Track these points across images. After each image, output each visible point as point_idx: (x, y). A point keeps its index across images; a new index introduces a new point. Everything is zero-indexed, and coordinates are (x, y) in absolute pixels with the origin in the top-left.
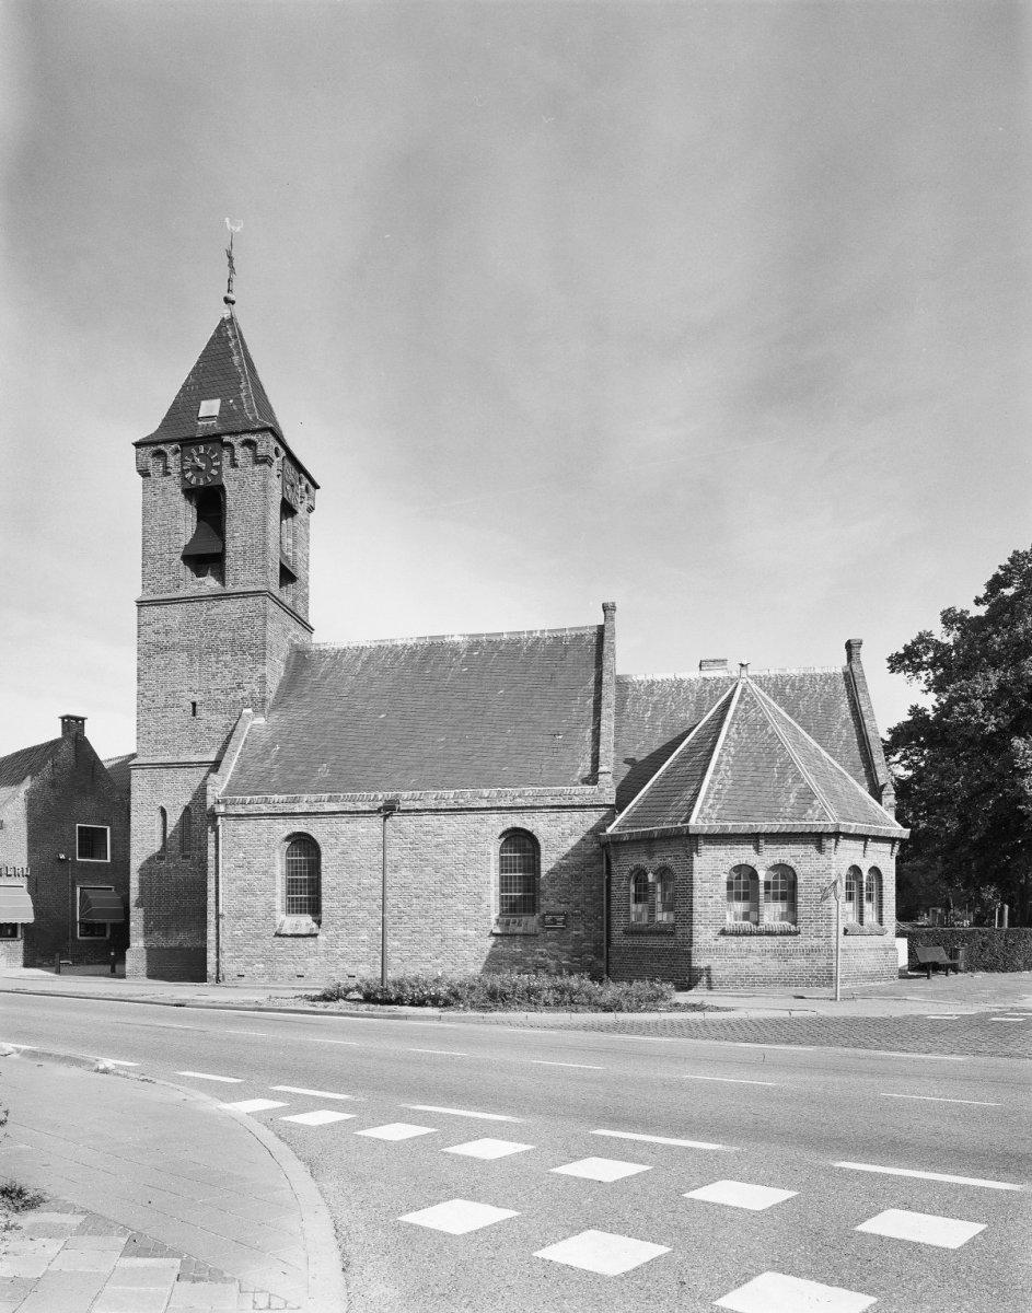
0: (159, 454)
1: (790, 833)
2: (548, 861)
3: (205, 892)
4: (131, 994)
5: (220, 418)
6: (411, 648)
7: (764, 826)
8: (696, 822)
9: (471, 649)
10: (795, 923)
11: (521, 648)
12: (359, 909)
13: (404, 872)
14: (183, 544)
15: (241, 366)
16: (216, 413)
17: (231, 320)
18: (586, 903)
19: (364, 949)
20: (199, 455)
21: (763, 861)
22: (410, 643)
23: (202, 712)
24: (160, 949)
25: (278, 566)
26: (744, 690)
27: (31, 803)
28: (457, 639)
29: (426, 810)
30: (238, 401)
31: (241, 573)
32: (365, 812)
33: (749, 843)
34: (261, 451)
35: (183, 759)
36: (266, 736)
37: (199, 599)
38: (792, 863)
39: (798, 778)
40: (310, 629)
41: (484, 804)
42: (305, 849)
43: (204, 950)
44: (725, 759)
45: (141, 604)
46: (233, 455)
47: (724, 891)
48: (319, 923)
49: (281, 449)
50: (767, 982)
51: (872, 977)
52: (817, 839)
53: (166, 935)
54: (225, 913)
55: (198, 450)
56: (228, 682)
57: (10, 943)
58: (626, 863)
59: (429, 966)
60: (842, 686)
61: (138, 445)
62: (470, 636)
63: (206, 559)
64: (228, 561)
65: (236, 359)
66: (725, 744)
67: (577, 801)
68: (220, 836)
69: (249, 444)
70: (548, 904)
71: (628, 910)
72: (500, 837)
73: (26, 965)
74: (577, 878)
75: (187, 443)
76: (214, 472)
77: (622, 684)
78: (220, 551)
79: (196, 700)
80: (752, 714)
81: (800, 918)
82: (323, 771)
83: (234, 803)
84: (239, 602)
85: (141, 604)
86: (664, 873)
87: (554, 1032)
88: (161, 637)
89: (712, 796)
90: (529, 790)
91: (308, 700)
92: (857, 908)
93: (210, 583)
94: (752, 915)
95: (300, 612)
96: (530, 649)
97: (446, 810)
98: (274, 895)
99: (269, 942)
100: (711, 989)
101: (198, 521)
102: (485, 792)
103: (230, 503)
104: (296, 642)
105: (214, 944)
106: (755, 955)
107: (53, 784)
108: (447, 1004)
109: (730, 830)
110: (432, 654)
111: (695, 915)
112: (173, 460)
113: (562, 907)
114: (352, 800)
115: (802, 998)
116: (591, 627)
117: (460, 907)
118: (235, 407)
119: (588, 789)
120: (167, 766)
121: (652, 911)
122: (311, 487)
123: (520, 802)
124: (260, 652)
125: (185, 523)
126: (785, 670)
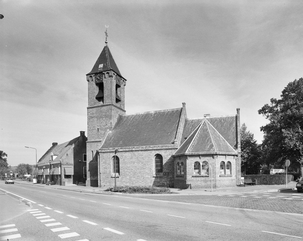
0: (91, 77)
1: (206, 155)
2: (164, 162)
3: (98, 168)
4: (88, 188)
5: (103, 68)
6: (143, 115)
7: (200, 153)
8: (187, 152)
9: (155, 114)
10: (208, 174)
11: (165, 114)
12: (127, 171)
13: (136, 164)
14: (96, 95)
15: (108, 56)
16: (102, 67)
17: (106, 47)
18: (172, 170)
19: (128, 180)
20: (98, 76)
21: (201, 160)
22: (143, 113)
23: (100, 131)
24: (92, 180)
25: (115, 99)
26: (204, 122)
27: (74, 149)
28: (152, 112)
29: (140, 150)
30: (107, 64)
31: (107, 101)
32: (128, 151)
33: (198, 157)
34: (110, 74)
35: (96, 140)
36: (111, 135)
37: (99, 107)
38: (207, 161)
39: (211, 142)
40: (125, 111)
41: (151, 149)
42: (117, 159)
43: (98, 180)
44: (196, 138)
45: (88, 108)
46: (105, 75)
47: (220, 167)
48: (119, 174)
49: (115, 73)
50: (202, 187)
51: (228, 186)
52: (212, 155)
53: (93, 177)
54: (101, 173)
55: (98, 75)
56: (104, 124)
57: (69, 179)
58: (176, 162)
59: (141, 184)
60: (235, 119)
61: (87, 75)
62: (155, 111)
63: (100, 98)
64: (104, 98)
65: (107, 55)
66: (197, 135)
67: (170, 148)
68: (100, 157)
69: (108, 73)
70: (165, 170)
71: (177, 172)
72: (155, 156)
73: (73, 183)
74: (170, 164)
75: (96, 74)
76: (101, 80)
77: (186, 121)
78: (102, 96)
79: (98, 128)
80: (205, 127)
81: (209, 173)
82: (121, 142)
83: (102, 150)
84: (106, 107)
85: (88, 108)
86: (182, 163)
87: (132, 198)
88: (92, 115)
89: (192, 146)
90: (160, 145)
91: (121, 127)
92: (224, 171)
93: (101, 103)
94: (199, 172)
95: (122, 108)
96: (167, 114)
97: (144, 150)
98: (111, 169)
99: (110, 179)
100: (191, 189)
101: (99, 90)
102: (151, 146)
103: (104, 86)
104: (121, 114)
105: (99, 179)
106: (199, 182)
107: (78, 146)
108: (125, 192)
109: (193, 154)
110: (147, 115)
111: (187, 173)
112: (94, 78)
113: (167, 171)
114: (125, 148)
115: (206, 191)
116: (180, 108)
117: (147, 171)
118: (106, 65)
119: (172, 145)
120: (93, 142)
121: (181, 171)
122: (124, 80)
123: (158, 148)
124: (110, 117)
125: (96, 90)
126: (222, 116)
